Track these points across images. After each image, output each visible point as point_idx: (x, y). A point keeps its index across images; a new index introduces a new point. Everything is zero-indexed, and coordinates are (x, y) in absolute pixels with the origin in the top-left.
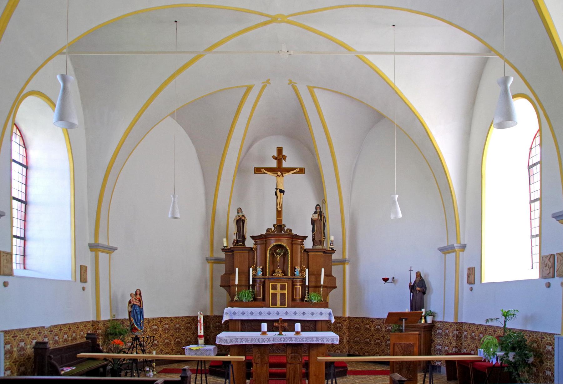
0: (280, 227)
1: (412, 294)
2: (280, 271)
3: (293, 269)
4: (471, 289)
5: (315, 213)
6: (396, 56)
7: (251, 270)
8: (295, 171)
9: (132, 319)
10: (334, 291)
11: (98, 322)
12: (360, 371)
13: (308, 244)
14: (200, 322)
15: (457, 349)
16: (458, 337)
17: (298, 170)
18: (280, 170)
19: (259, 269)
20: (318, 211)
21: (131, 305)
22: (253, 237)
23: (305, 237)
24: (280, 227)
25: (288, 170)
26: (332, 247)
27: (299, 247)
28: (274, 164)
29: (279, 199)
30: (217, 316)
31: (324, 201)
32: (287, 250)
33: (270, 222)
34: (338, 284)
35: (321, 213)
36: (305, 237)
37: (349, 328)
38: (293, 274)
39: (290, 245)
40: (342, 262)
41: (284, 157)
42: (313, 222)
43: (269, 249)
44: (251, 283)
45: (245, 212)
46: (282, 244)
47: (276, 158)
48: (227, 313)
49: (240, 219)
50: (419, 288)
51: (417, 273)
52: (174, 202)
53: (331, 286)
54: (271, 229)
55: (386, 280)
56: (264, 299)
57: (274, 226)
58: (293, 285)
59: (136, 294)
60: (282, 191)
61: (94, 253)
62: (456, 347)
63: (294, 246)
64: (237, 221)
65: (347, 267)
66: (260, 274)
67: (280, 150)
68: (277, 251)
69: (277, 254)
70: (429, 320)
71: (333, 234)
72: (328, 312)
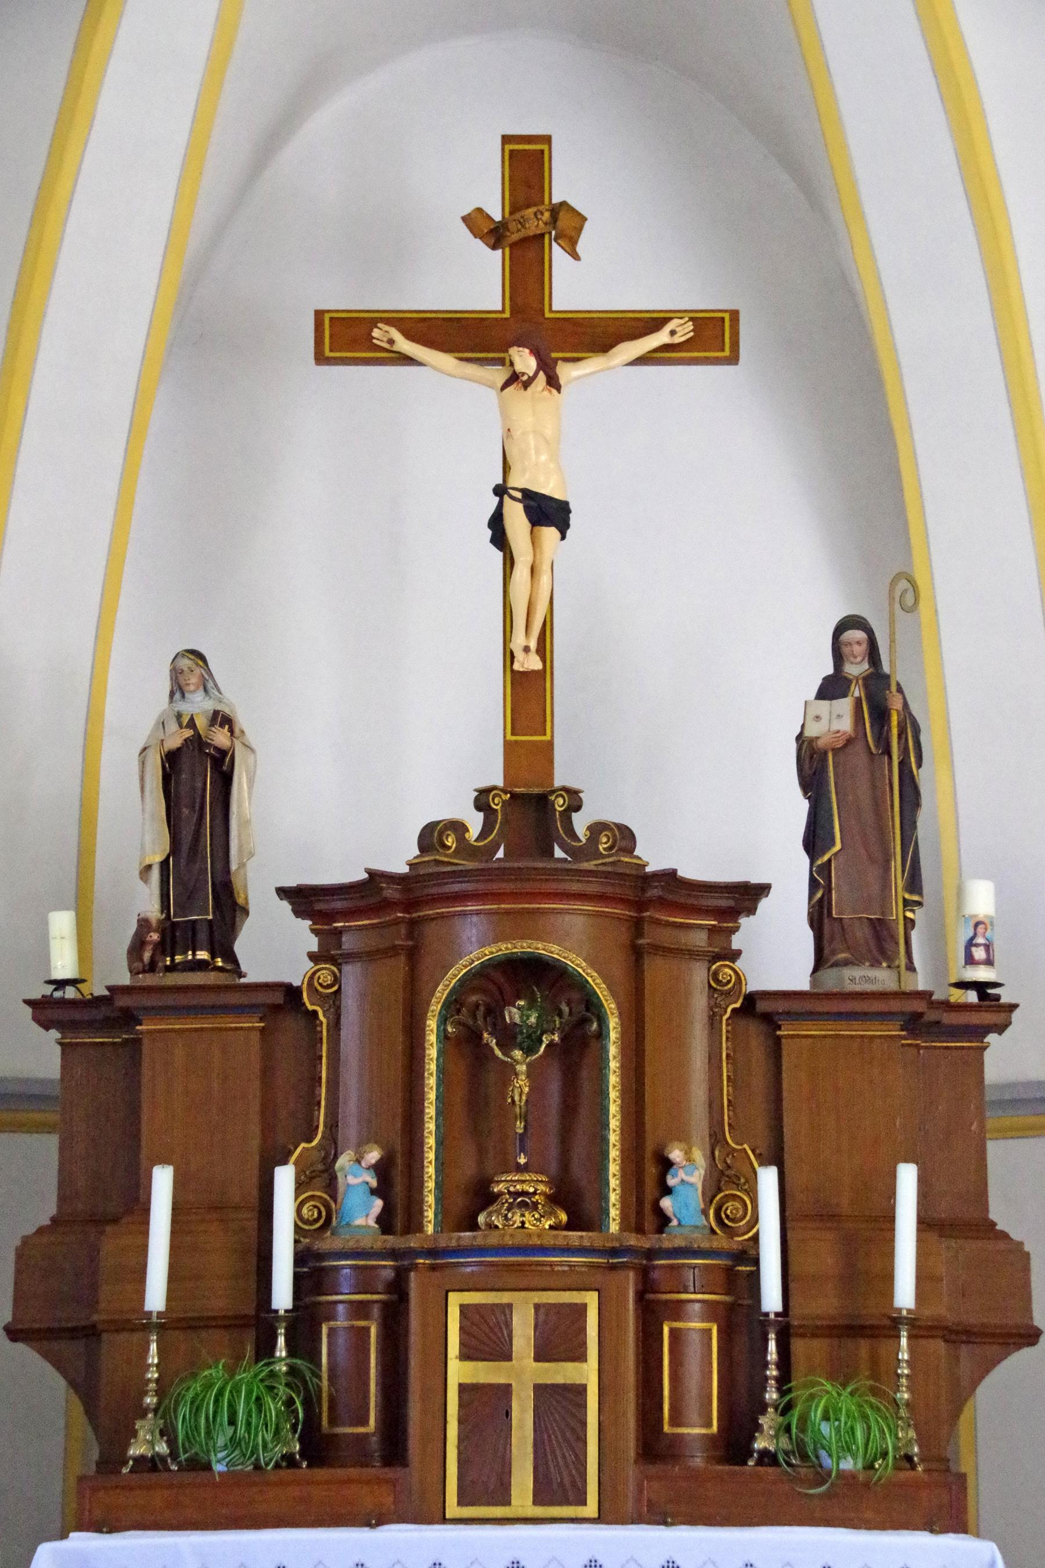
0: (530, 808)
3: (650, 1173)
5: (832, 688)
8: (661, 338)
10: (1021, 1359)
13: (776, 951)
17: (683, 330)
18: (527, 334)
19: (356, 1174)
22: (303, 899)
23: (747, 896)
25: (598, 334)
26: (982, 974)
27: (699, 974)
28: (479, 283)
29: (521, 572)
31: (906, 591)
32: (591, 1005)
35: (877, 683)
36: (747, 896)
39: (619, 968)
41: (567, 225)
42: (813, 765)
43: (442, 993)
44: (282, 1297)
47: (494, 235)
49: (197, 743)
54: (458, 827)
57: (482, 800)
58: (652, 1312)
60: (548, 513)
63: (656, 969)
64: (172, 760)
66: (362, 1211)
67: (526, 163)
68: (512, 1014)
69: (508, 1037)
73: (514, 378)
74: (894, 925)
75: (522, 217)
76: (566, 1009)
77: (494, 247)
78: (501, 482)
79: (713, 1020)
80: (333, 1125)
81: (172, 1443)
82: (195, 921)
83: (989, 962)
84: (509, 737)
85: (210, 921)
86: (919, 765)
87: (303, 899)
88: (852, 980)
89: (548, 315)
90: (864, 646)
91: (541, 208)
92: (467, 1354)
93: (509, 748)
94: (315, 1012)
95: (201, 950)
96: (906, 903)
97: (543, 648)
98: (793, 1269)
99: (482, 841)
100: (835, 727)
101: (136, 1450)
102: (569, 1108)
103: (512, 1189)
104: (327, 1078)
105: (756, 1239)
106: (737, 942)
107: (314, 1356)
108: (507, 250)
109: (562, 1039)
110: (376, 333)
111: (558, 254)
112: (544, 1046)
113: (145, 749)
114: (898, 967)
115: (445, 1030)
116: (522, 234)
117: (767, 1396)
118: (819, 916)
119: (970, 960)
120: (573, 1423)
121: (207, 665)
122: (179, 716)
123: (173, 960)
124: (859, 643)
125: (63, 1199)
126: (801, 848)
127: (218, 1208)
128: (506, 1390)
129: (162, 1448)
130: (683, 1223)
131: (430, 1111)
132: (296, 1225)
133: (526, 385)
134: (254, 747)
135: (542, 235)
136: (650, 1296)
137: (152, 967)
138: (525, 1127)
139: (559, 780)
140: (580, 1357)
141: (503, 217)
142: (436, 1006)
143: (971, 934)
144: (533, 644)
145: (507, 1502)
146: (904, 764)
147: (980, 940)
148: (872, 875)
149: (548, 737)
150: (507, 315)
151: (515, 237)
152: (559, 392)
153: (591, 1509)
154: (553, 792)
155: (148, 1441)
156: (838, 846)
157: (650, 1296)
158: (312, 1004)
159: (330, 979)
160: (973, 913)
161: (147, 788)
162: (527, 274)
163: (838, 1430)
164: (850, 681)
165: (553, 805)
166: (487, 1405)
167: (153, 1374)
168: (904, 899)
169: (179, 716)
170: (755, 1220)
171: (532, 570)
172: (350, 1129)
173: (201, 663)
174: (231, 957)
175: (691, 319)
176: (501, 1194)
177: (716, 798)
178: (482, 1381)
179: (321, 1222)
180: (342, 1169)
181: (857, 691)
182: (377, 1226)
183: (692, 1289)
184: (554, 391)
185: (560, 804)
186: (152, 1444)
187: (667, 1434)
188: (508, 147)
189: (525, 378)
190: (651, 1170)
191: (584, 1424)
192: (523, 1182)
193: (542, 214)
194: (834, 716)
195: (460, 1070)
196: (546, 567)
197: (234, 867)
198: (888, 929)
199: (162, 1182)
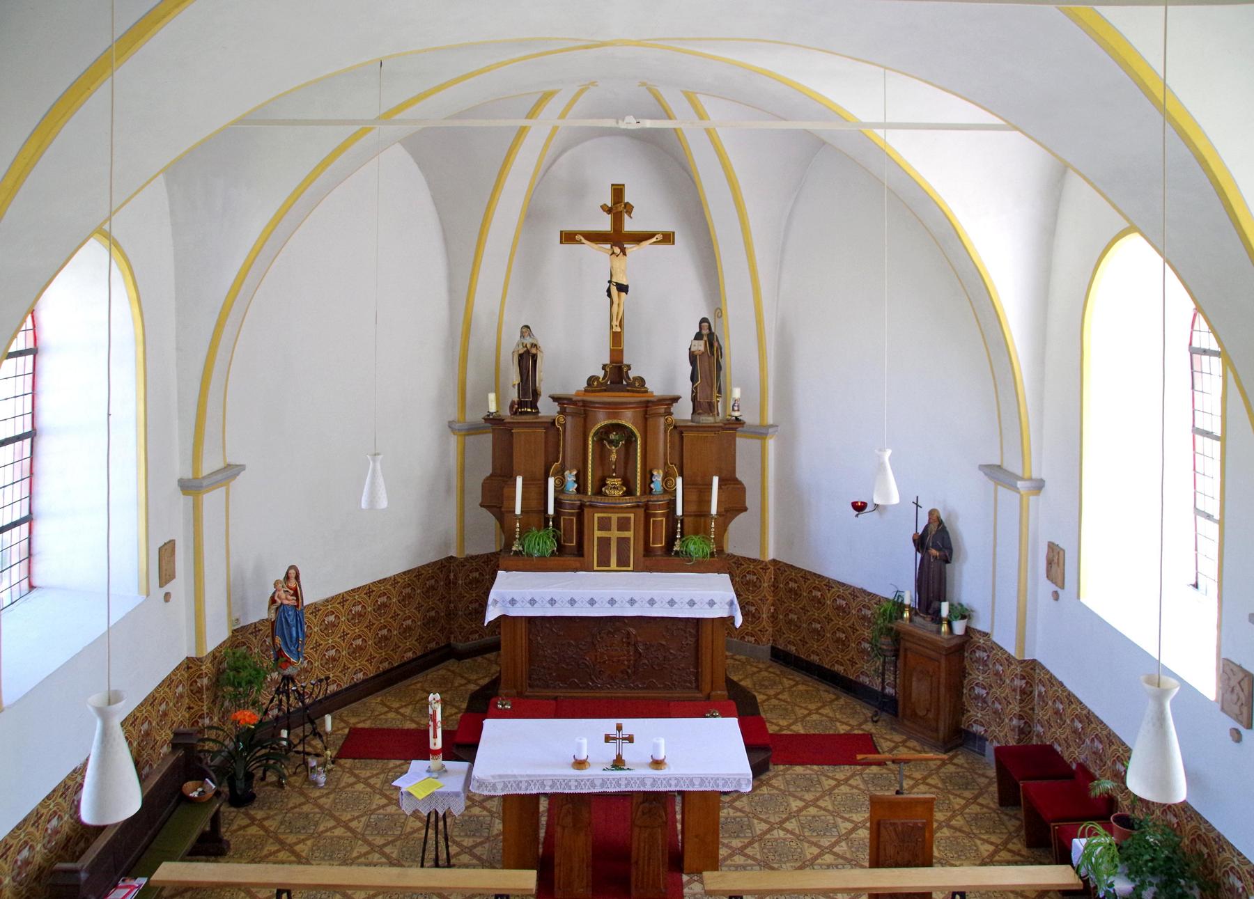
0: (617, 373)
1: (919, 555)
2: (617, 482)
3: (648, 477)
4: (1056, 596)
5: (698, 337)
6: (881, 120)
7: (551, 481)
8: (654, 240)
9: (278, 640)
10: (742, 515)
11: (200, 660)
12: (796, 737)
13: (683, 411)
14: (434, 721)
15: (1022, 723)
16: (1026, 694)
17: (659, 237)
18: (618, 239)
19: (570, 477)
20: (705, 332)
21: (274, 607)
23: (676, 399)
24: (617, 373)
25: (639, 238)
26: (736, 414)
27: (662, 420)
28: (604, 224)
29: (615, 306)
30: (472, 557)
31: (719, 312)
32: (632, 433)
33: (594, 362)
34: (751, 500)
35: (711, 335)
36: (676, 399)
37: (775, 586)
38: (647, 490)
40: (760, 433)
41: (629, 208)
42: (693, 358)
43: (593, 431)
44: (551, 511)
46: (623, 422)
47: (609, 211)
48: (496, 602)
49: (528, 352)
50: (935, 545)
51: (931, 513)
52: (374, 471)
53: (735, 503)
54: (597, 378)
55: (859, 507)
56: (580, 551)
57: (604, 367)
58: (647, 517)
59: (287, 577)
60: (623, 288)
61: (190, 498)
62: (1021, 717)
63: (650, 422)
64: (521, 356)
65: (771, 444)
66: (572, 487)
67: (618, 191)
70: (959, 627)
71: (738, 394)
72: (728, 600)
79: (666, 431)
93: (611, 351)
102: (626, 463)
118: (694, 399)
125: (494, 469)
137: (515, 413)
142: (591, 434)
153: (631, 568)
162: (618, 221)
166: (604, 543)
172: (568, 464)
174: (536, 408)
177: (664, 368)
199: (519, 480)
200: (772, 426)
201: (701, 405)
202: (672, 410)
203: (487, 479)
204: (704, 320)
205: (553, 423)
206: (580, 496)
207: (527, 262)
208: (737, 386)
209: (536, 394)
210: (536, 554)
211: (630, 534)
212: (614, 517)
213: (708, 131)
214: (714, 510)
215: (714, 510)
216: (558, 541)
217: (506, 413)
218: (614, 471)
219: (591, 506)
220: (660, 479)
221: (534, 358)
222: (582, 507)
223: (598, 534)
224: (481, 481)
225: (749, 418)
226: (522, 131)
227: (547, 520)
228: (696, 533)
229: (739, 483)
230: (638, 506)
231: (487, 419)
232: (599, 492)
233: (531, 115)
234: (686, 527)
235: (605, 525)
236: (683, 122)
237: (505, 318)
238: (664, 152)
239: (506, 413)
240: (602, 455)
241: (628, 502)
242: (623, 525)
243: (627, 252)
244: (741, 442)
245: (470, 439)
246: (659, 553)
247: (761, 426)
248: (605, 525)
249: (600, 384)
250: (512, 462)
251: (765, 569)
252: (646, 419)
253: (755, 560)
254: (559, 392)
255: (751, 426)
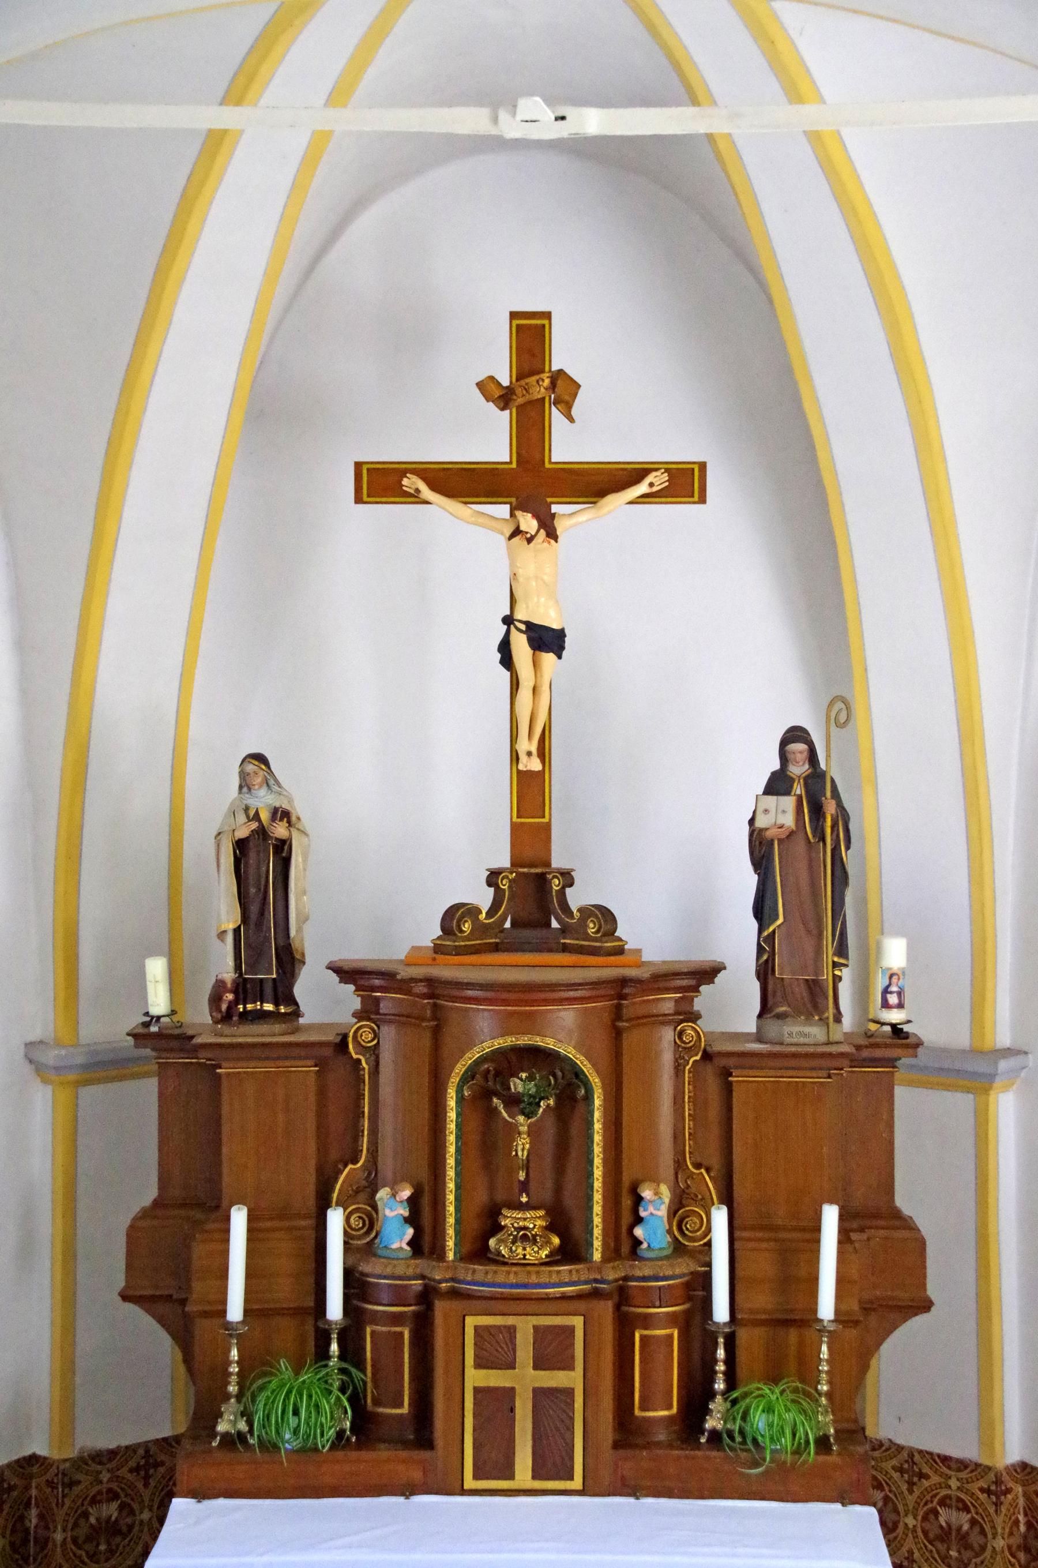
0: (533, 897)
2: (535, 1221)
3: (625, 1207)
7: (336, 1220)
8: (642, 488)
10: (918, 1322)
13: (733, 1007)
17: (658, 480)
18: (531, 487)
19: (393, 1207)
20: (799, 769)
22: (346, 973)
23: (708, 973)
24: (533, 897)
25: (597, 483)
26: (895, 1016)
27: (668, 1035)
28: (491, 441)
29: (525, 694)
30: (100, 1457)
31: (841, 710)
32: (578, 1074)
33: (462, 859)
34: (944, 1275)
35: (816, 778)
36: (708, 973)
38: (625, 1245)
39: (602, 1041)
40: (973, 1072)
41: (564, 390)
42: (761, 849)
43: (460, 1069)
44: (335, 1309)
45: (296, 786)
46: (549, 1043)
47: (504, 398)
49: (262, 832)
53: (893, 1283)
54: (472, 911)
56: (421, 1430)
57: (493, 877)
60: (547, 640)
63: (632, 1039)
64: (241, 845)
65: (1007, 1107)
66: (397, 1236)
67: (530, 334)
68: (517, 1085)
69: (513, 1102)
71: (902, 956)
73: (517, 532)
74: (825, 983)
75: (527, 384)
76: (559, 1074)
77: (502, 409)
78: (508, 613)
79: (678, 1069)
80: (373, 1153)
81: (250, 1423)
82: (261, 980)
83: (900, 1006)
84: (515, 819)
85: (274, 979)
86: (848, 848)
87: (346, 973)
88: (790, 1034)
89: (547, 465)
90: (806, 754)
91: (542, 376)
92: (480, 1364)
93: (515, 828)
94: (359, 1061)
95: (268, 1002)
96: (835, 965)
97: (543, 752)
98: (739, 1273)
99: (491, 918)
100: (780, 821)
101: (222, 1427)
103: (516, 1225)
104: (369, 1112)
105: (709, 1244)
106: (698, 1004)
107: (360, 1365)
108: (514, 410)
109: (556, 1103)
110: (405, 482)
111: (556, 416)
112: (541, 1110)
113: (219, 834)
114: (828, 1018)
115: (463, 1095)
116: (528, 397)
117: (716, 1386)
118: (764, 972)
119: (885, 1005)
120: (564, 1416)
121: (269, 767)
122: (247, 809)
123: (245, 1008)
124: (801, 752)
126: (752, 914)
127: (283, 1214)
128: (511, 1365)
129: (242, 1426)
130: (652, 1246)
131: (451, 1161)
132: (345, 1233)
133: (530, 540)
134: (309, 832)
135: (544, 399)
136: (625, 1309)
137: (227, 1018)
138: (527, 1175)
139: (557, 863)
140: (571, 1367)
141: (511, 382)
142: (454, 1080)
143: (887, 983)
144: (534, 748)
145: (511, 1477)
146: (836, 850)
147: (894, 988)
148: (809, 944)
149: (546, 820)
150: (514, 466)
151: (520, 401)
152: (556, 541)
153: (577, 1483)
154: (549, 873)
155: (231, 1421)
156: (780, 920)
157: (625, 1309)
158: (356, 1053)
159: (371, 1036)
160: (890, 966)
161: (222, 868)
162: (530, 433)
163: (770, 1425)
164: (792, 780)
165: (551, 883)
166: (496, 1405)
167: (234, 1369)
168: (834, 962)
169: (247, 809)
170: (709, 1230)
171: (534, 689)
172: (387, 1164)
173: (263, 767)
174: (292, 1001)
175: (667, 470)
176: (505, 1226)
177: (673, 876)
178: (492, 1385)
179: (365, 1229)
180: (381, 1199)
181: (798, 789)
182: (408, 1248)
183: (657, 1304)
184: (552, 542)
185: (556, 884)
186: (234, 1423)
187: (637, 1418)
188: (515, 322)
189: (529, 536)
190: (627, 1202)
191: (572, 1419)
192: (525, 1219)
193: (543, 380)
194: (780, 811)
195: (474, 1124)
196: (545, 688)
197: (293, 933)
198: (821, 988)
199: (239, 1219)
200: (1008, 1052)
201: (789, 986)
202: (699, 1004)
203: (145, 1214)
204: (795, 735)
205: (342, 1045)
206: (421, 1265)
207: (258, 575)
208: (897, 934)
209: (289, 961)
210: (289, 1442)
211: (572, 1379)
212: (525, 1327)
213: (814, 138)
214: (826, 1308)
215: (826, 1308)
216: (356, 1401)
217: (199, 1016)
218: (524, 1187)
219: (455, 1294)
220: (663, 1212)
221: (283, 850)
222: (427, 1296)
223: (475, 1377)
224: (125, 1221)
225: (935, 1023)
226: (215, 144)
227: (323, 1338)
228: (774, 1378)
229: (906, 1224)
230: (596, 1294)
231: (140, 1037)
232: (479, 1252)
233: (238, 91)
234: (742, 1357)
235: (496, 1351)
236: (740, 114)
237: (196, 728)
238: (680, 209)
239: (199, 1016)
240: (487, 1143)
241: (568, 1279)
242: (552, 1351)
243: (561, 526)
244: (906, 1099)
245: (88, 1093)
246: (662, 1436)
247: (976, 1052)
248: (496, 1351)
249: (481, 930)
250: (217, 1163)
251: (997, 1490)
252: (618, 1034)
253: (962, 1465)
254: (360, 951)
255: (945, 1052)
